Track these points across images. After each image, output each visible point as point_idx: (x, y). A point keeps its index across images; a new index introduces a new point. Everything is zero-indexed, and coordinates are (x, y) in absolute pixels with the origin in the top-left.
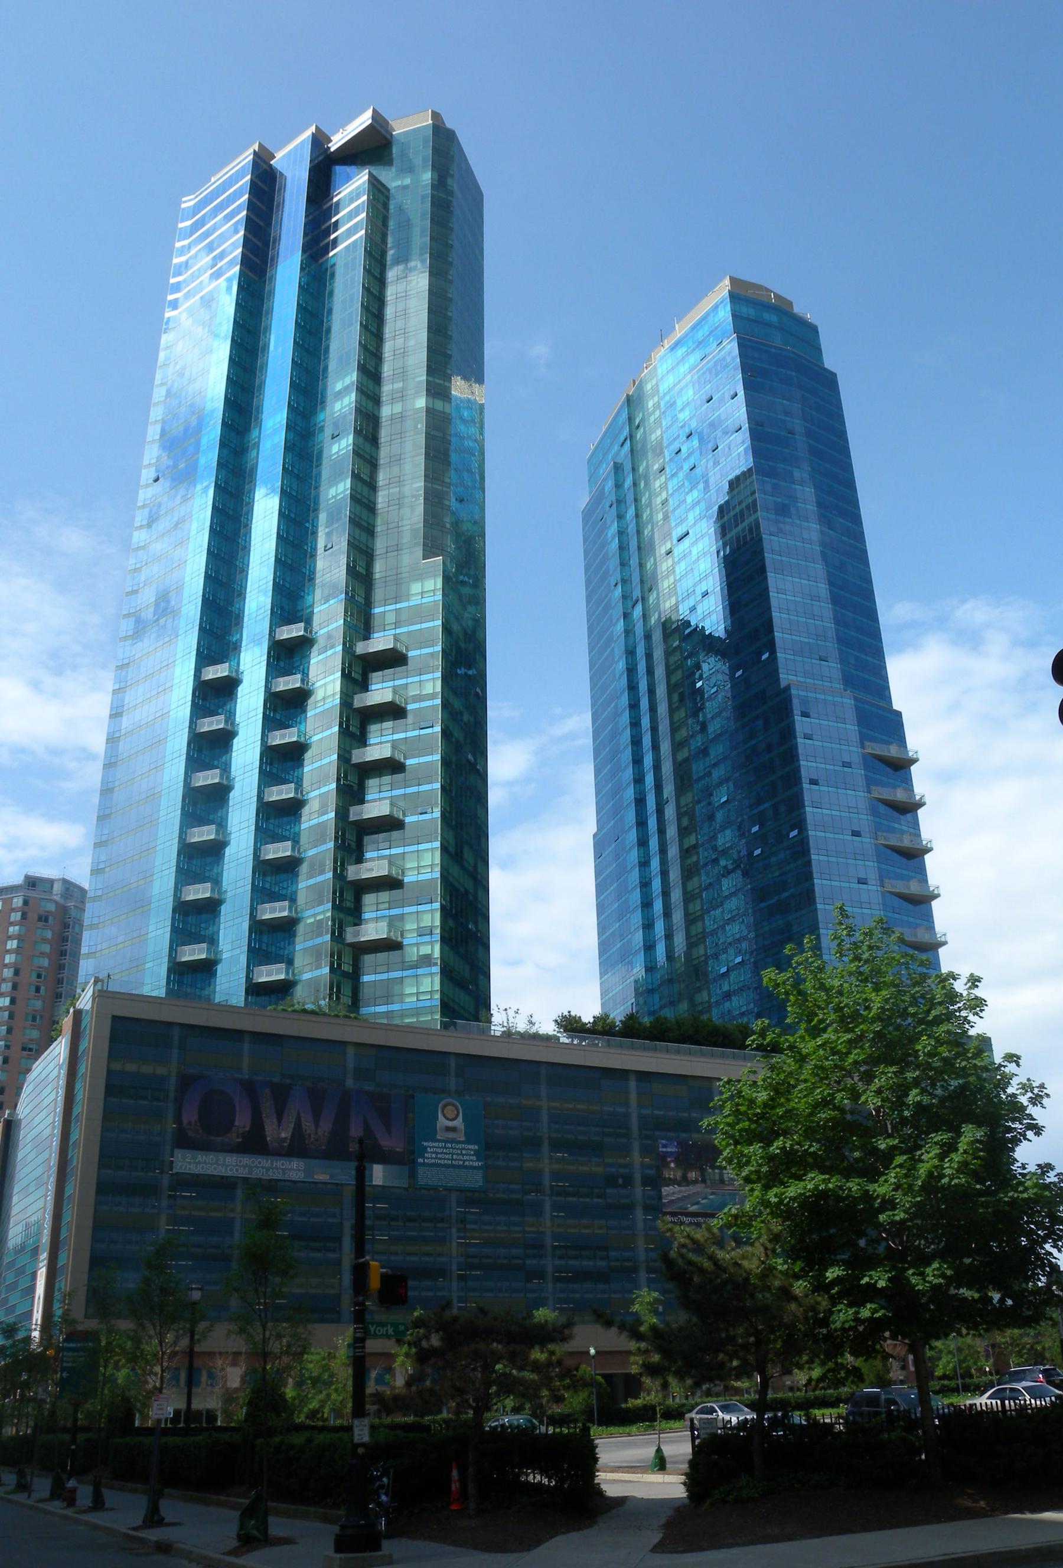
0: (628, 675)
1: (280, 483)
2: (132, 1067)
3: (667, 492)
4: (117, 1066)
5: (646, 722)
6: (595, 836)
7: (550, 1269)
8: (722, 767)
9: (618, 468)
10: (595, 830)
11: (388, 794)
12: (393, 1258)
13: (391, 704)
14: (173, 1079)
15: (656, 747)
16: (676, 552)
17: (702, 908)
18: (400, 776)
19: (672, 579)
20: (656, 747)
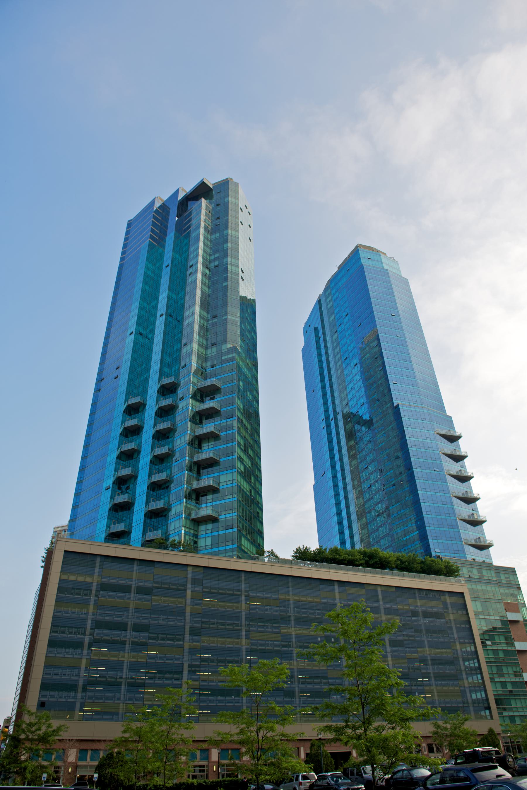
0: (320, 377)
1: (159, 366)
2: (73, 578)
3: (347, 392)
4: (65, 577)
5: (341, 485)
6: (314, 486)
7: (297, 690)
8: (371, 455)
9: (316, 329)
10: (314, 483)
11: (210, 535)
12: (210, 684)
13: (212, 433)
14: (95, 584)
15: (344, 479)
16: (338, 331)
17: (367, 522)
18: (216, 495)
19: (345, 393)
20: (344, 479)
